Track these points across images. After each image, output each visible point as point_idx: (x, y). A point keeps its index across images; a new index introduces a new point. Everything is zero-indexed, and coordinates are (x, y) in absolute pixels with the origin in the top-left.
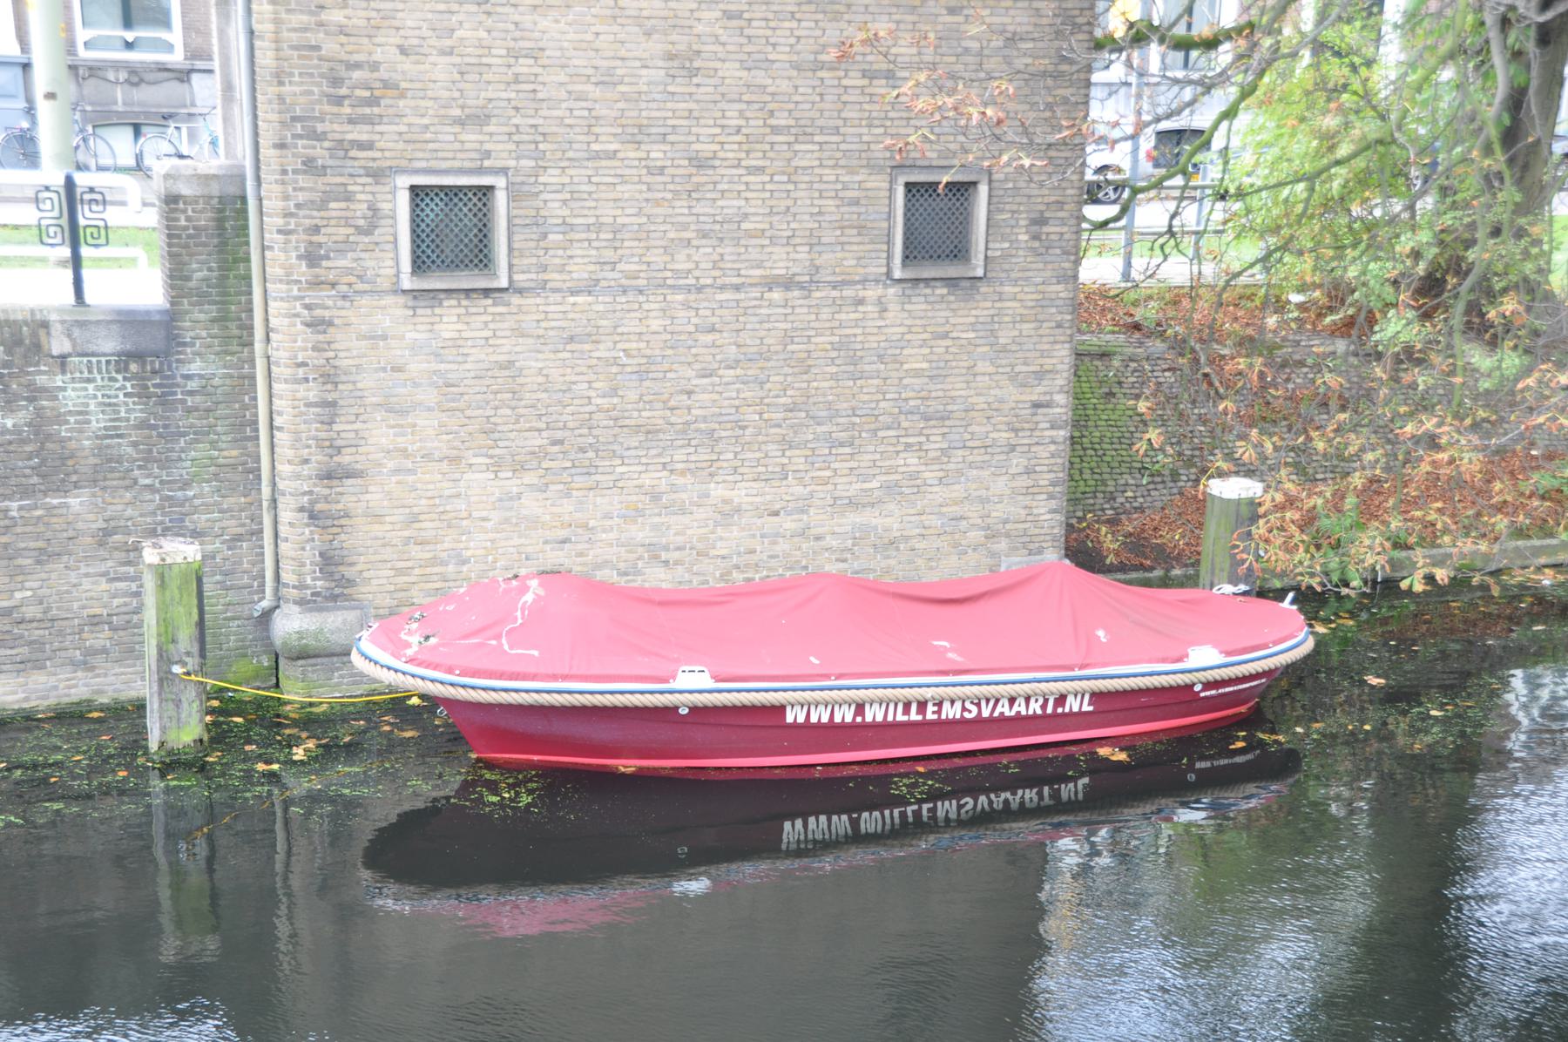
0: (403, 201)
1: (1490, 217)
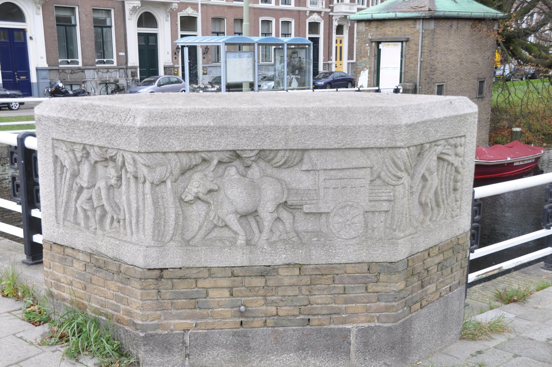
1: (62, 330)
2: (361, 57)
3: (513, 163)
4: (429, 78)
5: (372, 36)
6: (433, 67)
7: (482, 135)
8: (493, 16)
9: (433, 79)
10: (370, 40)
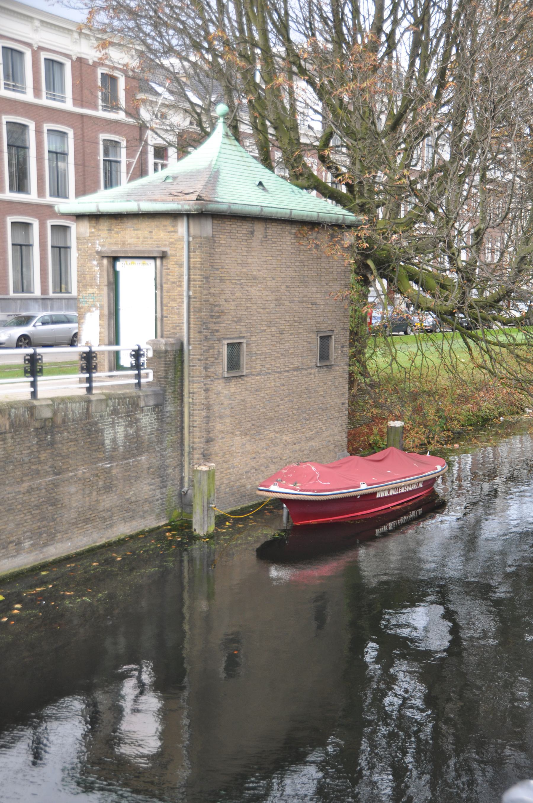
0: (225, 348)
2: (85, 286)
3: (375, 494)
4: (207, 329)
5: (102, 246)
6: (216, 308)
7: (334, 435)
8: (338, 219)
9: (217, 331)
10: (98, 253)
